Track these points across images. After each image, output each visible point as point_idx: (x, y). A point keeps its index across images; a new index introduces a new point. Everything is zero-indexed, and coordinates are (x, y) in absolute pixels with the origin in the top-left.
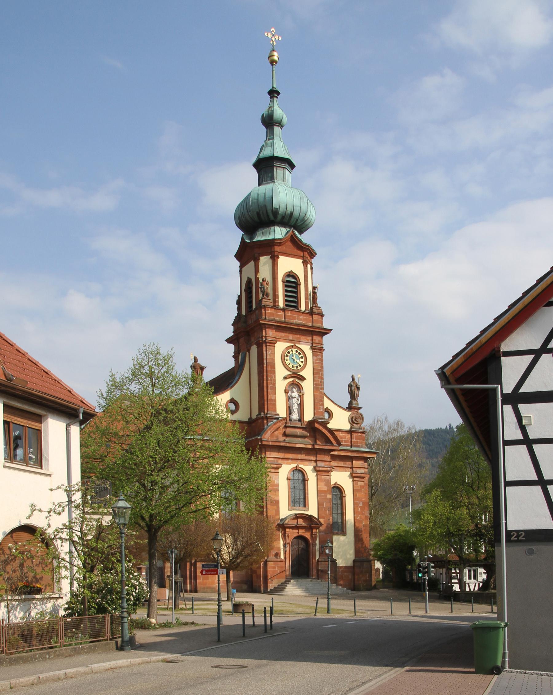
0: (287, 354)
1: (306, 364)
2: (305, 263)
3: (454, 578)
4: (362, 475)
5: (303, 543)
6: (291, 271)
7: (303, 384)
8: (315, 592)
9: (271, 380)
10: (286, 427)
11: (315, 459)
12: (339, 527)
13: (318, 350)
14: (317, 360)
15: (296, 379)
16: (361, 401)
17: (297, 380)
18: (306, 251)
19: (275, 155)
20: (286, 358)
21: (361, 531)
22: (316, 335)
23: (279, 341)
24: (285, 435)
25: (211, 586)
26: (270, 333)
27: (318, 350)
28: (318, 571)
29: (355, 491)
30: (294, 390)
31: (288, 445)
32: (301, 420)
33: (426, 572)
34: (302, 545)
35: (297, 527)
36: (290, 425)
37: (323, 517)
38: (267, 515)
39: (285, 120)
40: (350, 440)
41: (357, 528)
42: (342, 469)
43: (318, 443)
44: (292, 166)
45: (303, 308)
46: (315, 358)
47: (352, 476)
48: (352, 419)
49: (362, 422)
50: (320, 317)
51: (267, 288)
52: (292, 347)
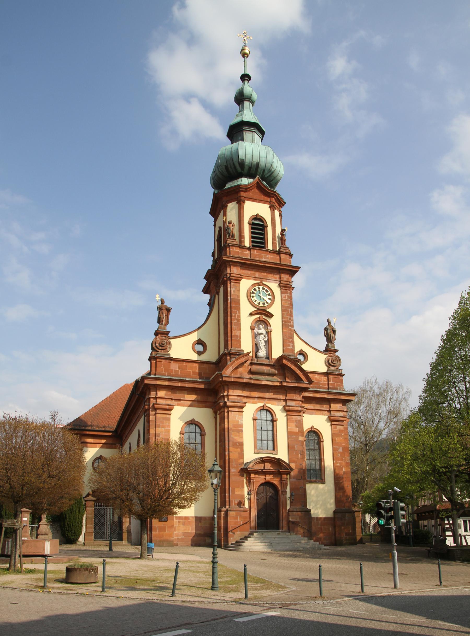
0: (253, 290)
1: (274, 301)
2: (272, 208)
3: (448, 530)
4: (341, 419)
5: (272, 491)
6: (258, 214)
7: (271, 321)
8: (279, 547)
9: (235, 316)
10: (252, 364)
11: (284, 398)
12: (317, 475)
13: (286, 287)
14: (285, 297)
15: (263, 314)
16: (337, 345)
17: (264, 317)
18: (273, 197)
19: (244, 120)
20: (252, 295)
21: (342, 478)
22: (285, 273)
23: (245, 278)
24: (251, 372)
25: (168, 538)
26: (235, 271)
27: (286, 287)
28: (289, 522)
29: (333, 436)
30: (261, 326)
31: (253, 382)
32: (268, 357)
33: (391, 517)
34: (270, 492)
35: (264, 472)
36: (256, 362)
37: (294, 462)
38: (229, 459)
39: (255, 96)
40: (327, 383)
41: (337, 474)
42: (319, 412)
43: (287, 380)
44: (262, 133)
45: (270, 247)
46: (283, 295)
47: (330, 420)
48: (328, 361)
49: (340, 365)
50: (288, 256)
51: (233, 229)
52: (259, 284)
